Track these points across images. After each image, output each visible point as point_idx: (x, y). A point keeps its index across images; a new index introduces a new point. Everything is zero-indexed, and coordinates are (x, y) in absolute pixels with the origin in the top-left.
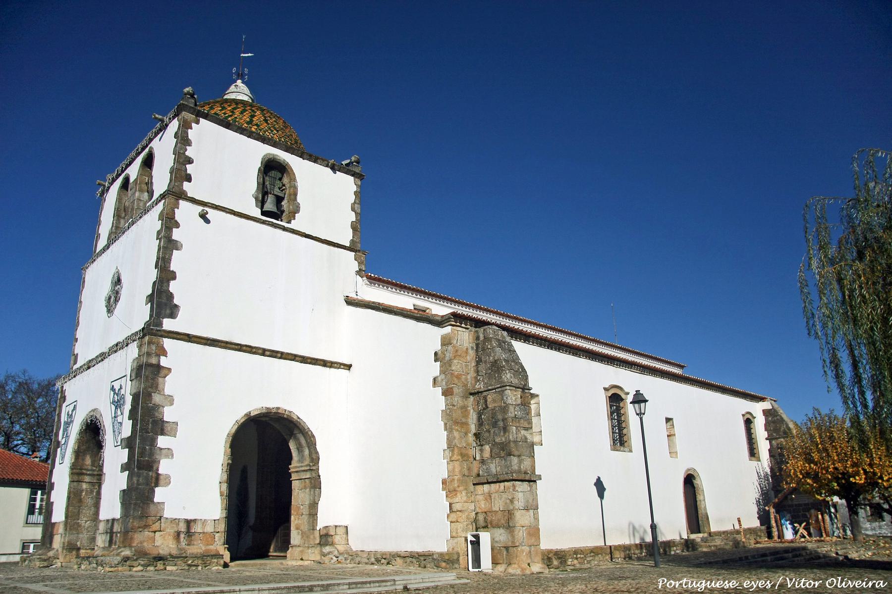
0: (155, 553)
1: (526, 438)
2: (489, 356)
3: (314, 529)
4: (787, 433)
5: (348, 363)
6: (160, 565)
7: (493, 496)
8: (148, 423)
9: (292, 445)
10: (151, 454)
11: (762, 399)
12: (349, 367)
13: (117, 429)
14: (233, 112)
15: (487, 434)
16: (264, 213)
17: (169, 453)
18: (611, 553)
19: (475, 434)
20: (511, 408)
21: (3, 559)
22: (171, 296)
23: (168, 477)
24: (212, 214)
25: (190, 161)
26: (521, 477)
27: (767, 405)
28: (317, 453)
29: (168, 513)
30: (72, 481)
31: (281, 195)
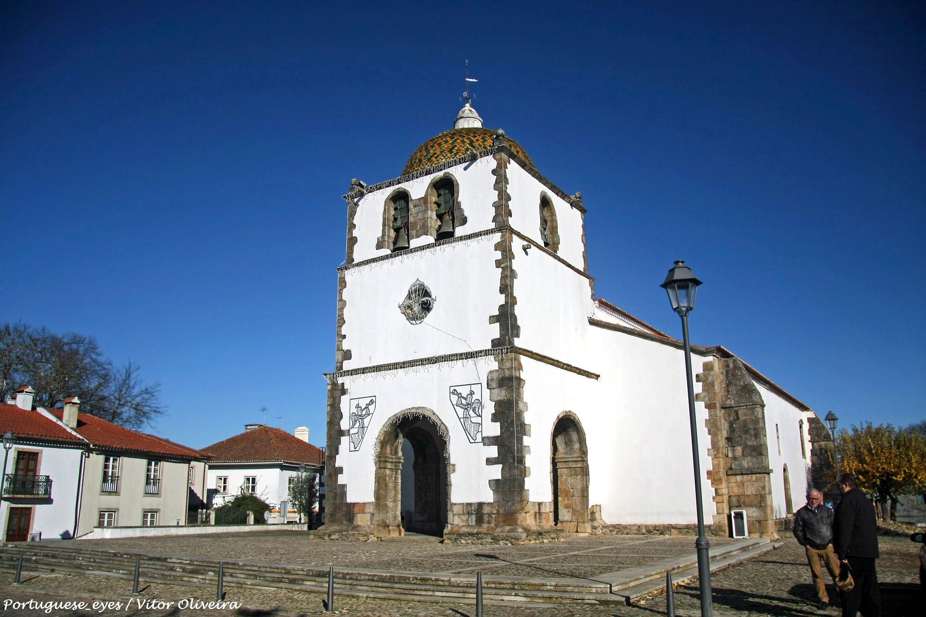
2: (740, 380)
4: (827, 438)
7: (746, 484)
11: (803, 408)
15: (739, 439)
19: (727, 438)
27: (810, 414)
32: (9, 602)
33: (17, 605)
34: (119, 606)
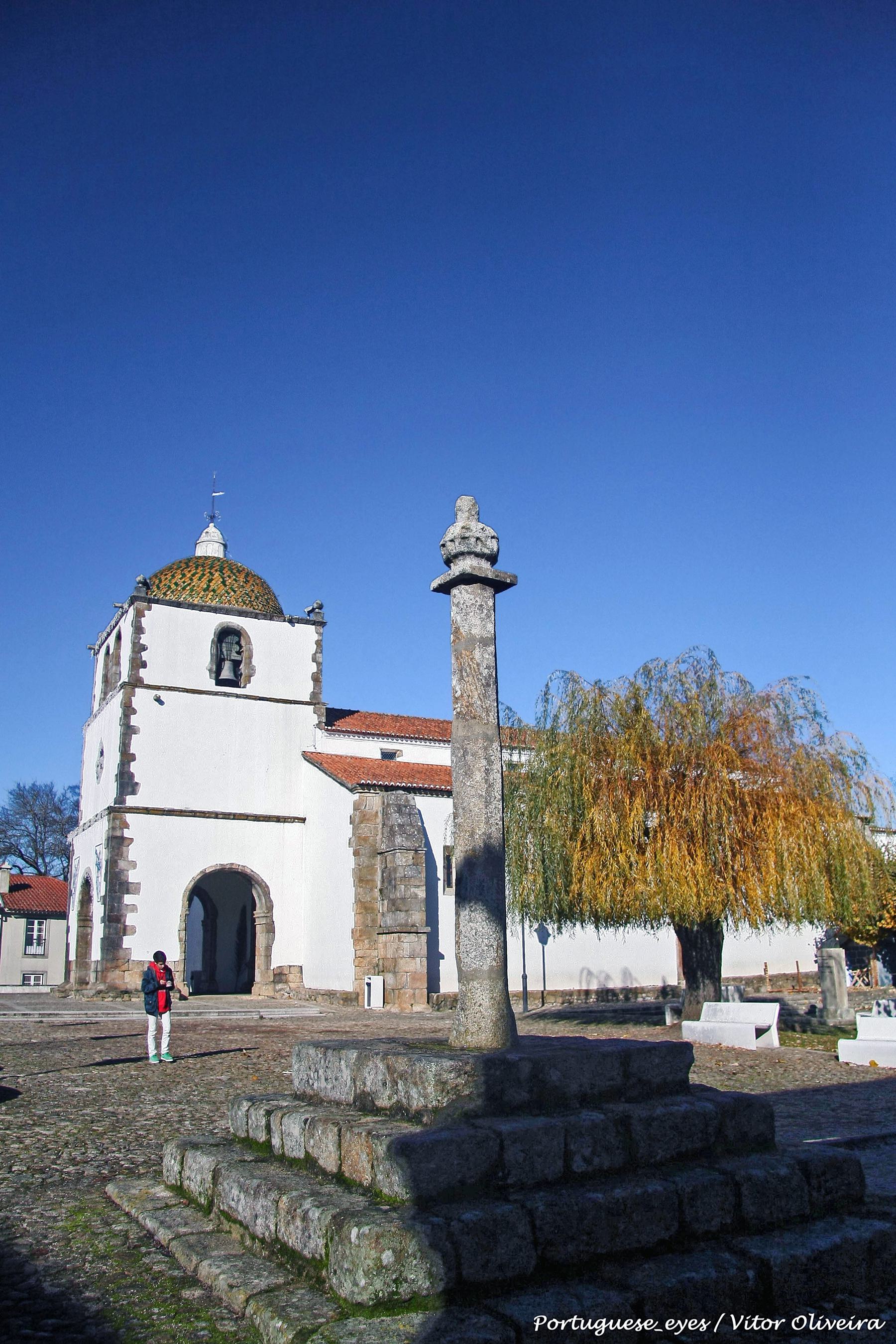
0: (123, 988)
1: (416, 895)
3: (268, 968)
5: (302, 816)
6: (126, 997)
8: (118, 886)
9: (254, 892)
10: (119, 910)
12: (303, 820)
13: (99, 889)
14: (191, 579)
16: (220, 682)
17: (134, 908)
18: (543, 998)
20: (401, 870)
21: (3, 990)
22: (132, 776)
23: (134, 928)
24: (163, 694)
25: (144, 648)
26: (408, 929)
28: (271, 901)
29: (135, 957)
30: (79, 927)
31: (239, 658)
32: (542, 1320)
33: (553, 1325)
34: (704, 1325)
